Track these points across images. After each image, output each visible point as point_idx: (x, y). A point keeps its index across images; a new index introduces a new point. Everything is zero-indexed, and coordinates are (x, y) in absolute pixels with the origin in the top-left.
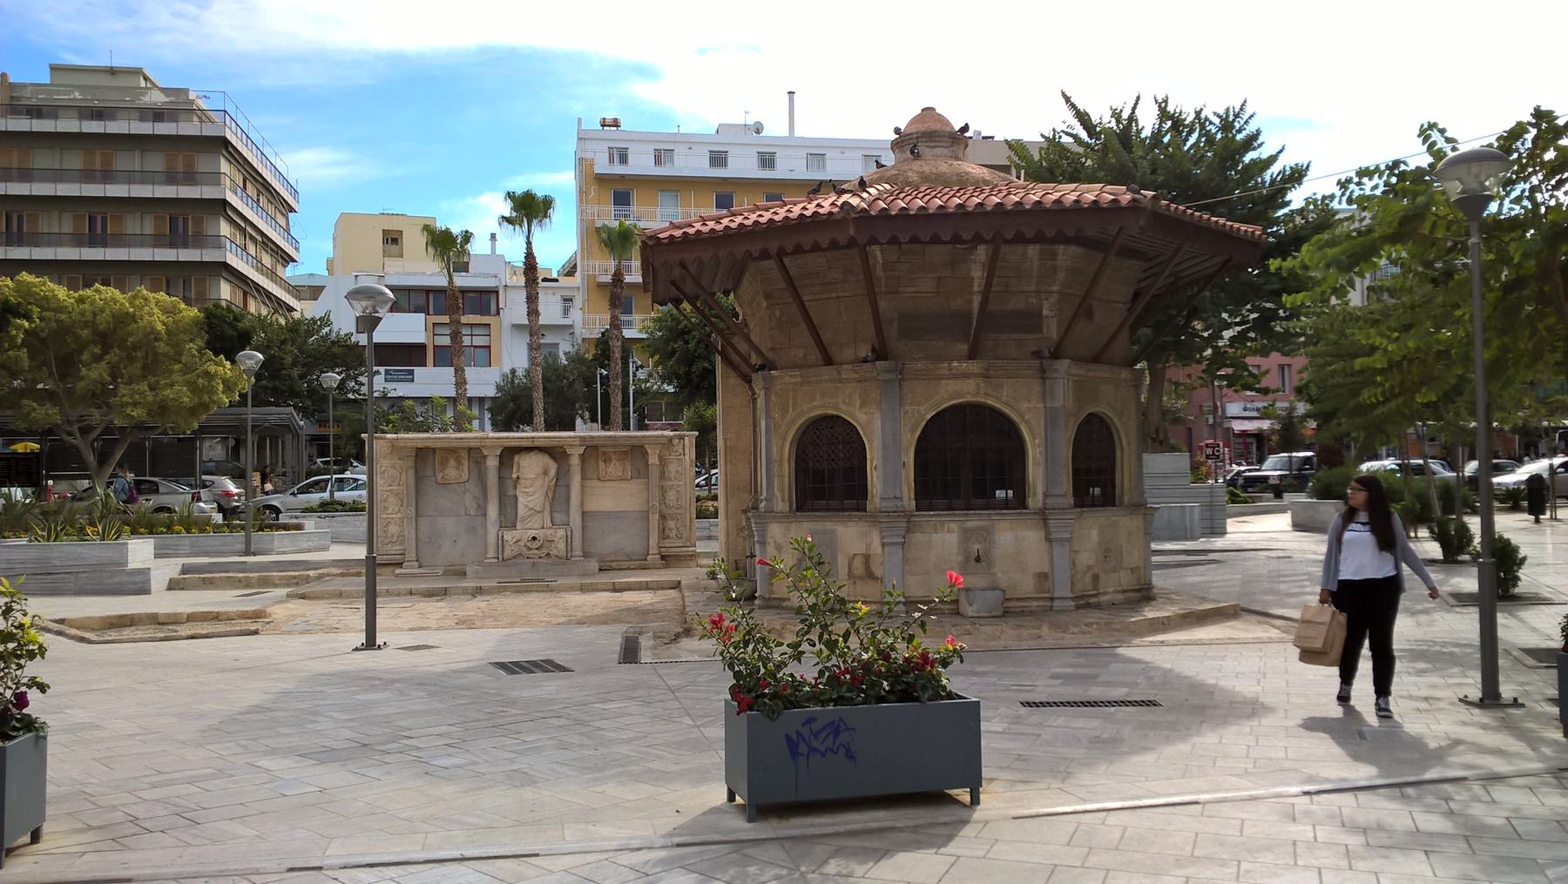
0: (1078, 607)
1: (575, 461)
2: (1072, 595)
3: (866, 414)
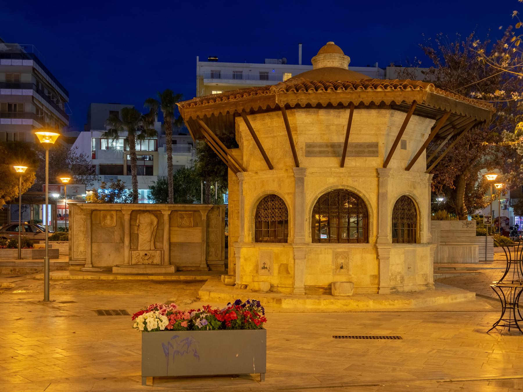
0: (392, 293)
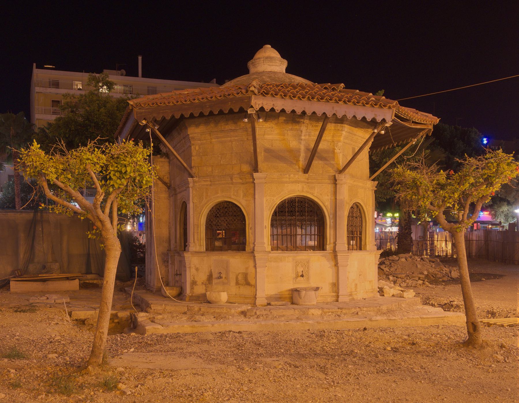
3: (246, 201)
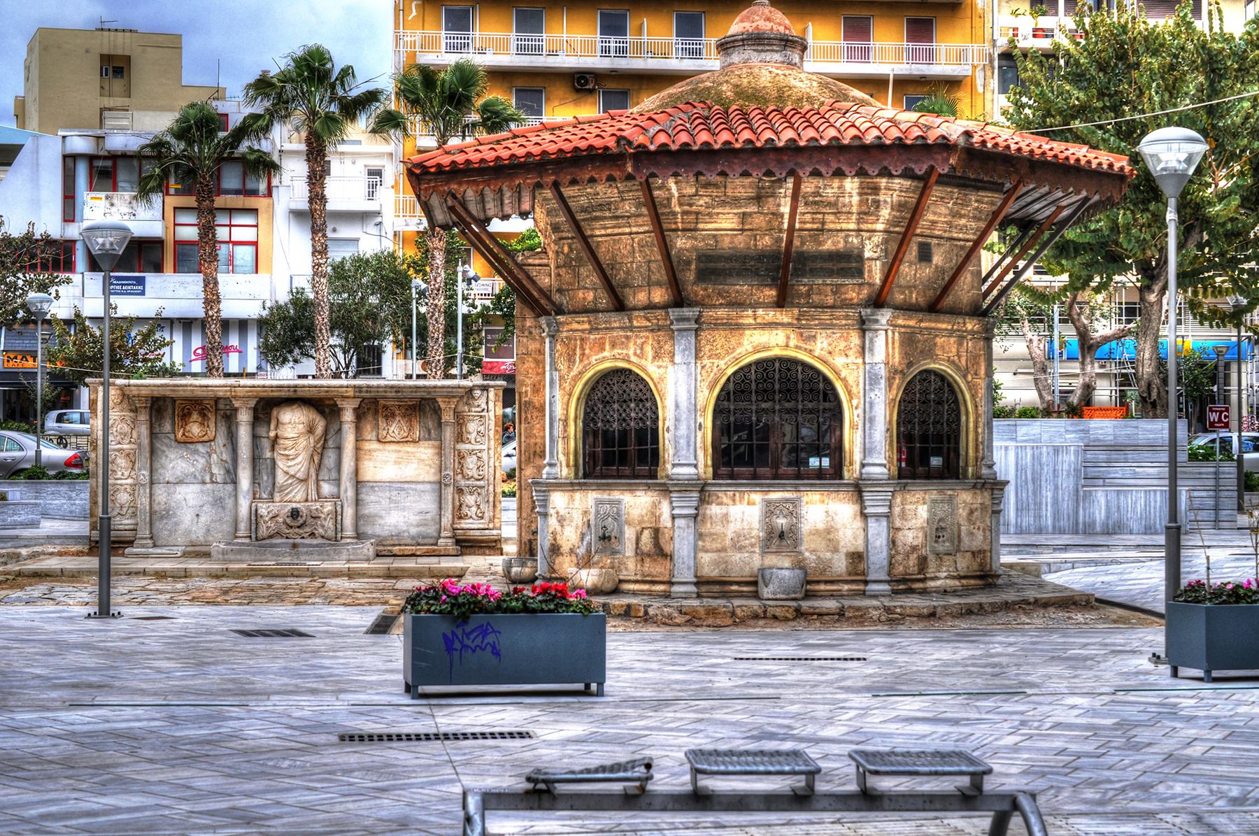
1: (348, 416)
2: (888, 578)
